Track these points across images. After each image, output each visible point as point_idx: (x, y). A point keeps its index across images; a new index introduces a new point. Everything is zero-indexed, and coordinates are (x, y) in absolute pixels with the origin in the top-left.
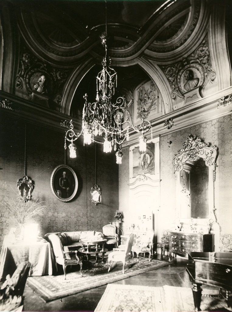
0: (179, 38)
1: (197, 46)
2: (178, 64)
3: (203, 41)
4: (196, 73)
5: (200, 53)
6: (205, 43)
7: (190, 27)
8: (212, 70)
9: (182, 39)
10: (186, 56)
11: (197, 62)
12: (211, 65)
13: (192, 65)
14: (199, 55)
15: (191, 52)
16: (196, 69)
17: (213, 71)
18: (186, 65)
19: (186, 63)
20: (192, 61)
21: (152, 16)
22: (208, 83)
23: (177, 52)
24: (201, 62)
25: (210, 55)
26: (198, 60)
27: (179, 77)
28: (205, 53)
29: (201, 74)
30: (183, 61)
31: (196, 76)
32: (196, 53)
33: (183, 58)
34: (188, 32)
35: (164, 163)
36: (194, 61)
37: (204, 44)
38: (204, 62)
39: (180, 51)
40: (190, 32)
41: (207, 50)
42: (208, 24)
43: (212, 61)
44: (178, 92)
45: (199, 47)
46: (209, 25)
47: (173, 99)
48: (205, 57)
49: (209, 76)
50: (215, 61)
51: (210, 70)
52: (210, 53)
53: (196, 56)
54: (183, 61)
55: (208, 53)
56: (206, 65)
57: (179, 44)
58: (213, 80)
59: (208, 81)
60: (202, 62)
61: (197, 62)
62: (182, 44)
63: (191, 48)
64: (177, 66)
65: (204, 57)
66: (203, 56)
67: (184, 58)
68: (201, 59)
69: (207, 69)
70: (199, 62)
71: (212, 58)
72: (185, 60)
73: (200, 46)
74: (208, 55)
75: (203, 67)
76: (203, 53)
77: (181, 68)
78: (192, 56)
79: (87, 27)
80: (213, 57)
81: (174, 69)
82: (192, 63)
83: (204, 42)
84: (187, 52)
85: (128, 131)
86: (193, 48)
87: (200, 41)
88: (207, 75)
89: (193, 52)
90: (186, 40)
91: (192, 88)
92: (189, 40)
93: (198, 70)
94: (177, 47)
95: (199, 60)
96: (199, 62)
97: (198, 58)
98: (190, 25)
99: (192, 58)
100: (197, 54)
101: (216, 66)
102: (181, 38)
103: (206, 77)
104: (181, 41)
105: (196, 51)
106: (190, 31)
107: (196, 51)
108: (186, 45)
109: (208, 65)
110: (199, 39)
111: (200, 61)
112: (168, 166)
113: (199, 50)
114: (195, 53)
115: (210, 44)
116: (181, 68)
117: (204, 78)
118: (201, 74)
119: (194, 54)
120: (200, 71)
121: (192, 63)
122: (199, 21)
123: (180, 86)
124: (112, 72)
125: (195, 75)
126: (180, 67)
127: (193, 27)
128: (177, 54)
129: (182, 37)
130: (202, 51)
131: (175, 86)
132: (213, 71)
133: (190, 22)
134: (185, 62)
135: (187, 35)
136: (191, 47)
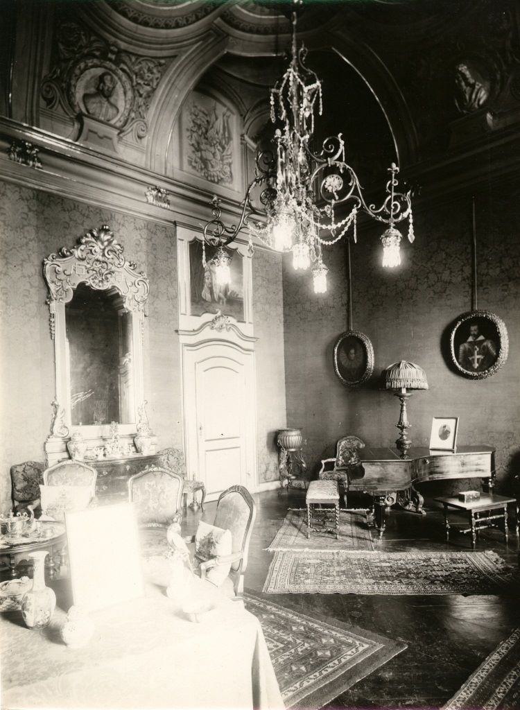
0: (142, 6)
1: (149, 55)
2: (98, 41)
3: (163, 58)
4: (117, 95)
5: (146, 71)
6: (162, 65)
7: (170, 17)
8: (144, 118)
9: (143, 13)
10: (123, 45)
11: (131, 79)
12: (148, 109)
13: (120, 72)
14: (142, 72)
15: (136, 52)
16: (122, 89)
17: (145, 120)
18: (110, 60)
19: (113, 57)
20: (125, 68)
21: (364, 79)
22: (130, 134)
23: (118, 20)
24: (136, 86)
25: (156, 91)
26: (134, 77)
27: (82, 65)
28: (152, 80)
29: (126, 105)
30: (112, 48)
31: (116, 100)
32: (140, 63)
33: (115, 42)
34: (161, 19)
35: (290, 308)
36: (128, 71)
37: (160, 65)
38: (141, 92)
39: (122, 26)
40: (162, 24)
41: (157, 79)
42: (190, 47)
43: (152, 103)
44: (63, 92)
45: (152, 61)
46: (186, 52)
47: (45, 99)
48: (148, 85)
49: (135, 124)
50: (157, 108)
51: (142, 113)
52: (159, 87)
53: (136, 68)
54: (112, 48)
55: (155, 84)
56: (140, 99)
57: (131, 15)
58: (140, 137)
59: (132, 130)
60: (138, 87)
61: (131, 79)
62: (135, 20)
63: (141, 47)
64: (94, 41)
65: (146, 83)
66: (146, 80)
67: (115, 45)
68: (140, 81)
69: (139, 107)
70: (135, 83)
71: (154, 103)
72: (116, 50)
73: (153, 60)
74: (152, 87)
75: (135, 97)
76: (148, 76)
77: (97, 53)
78: (131, 60)
79: (489, 116)
80: (157, 99)
81: (84, 41)
82: (123, 70)
83: (163, 61)
84: (130, 43)
85: (316, 224)
86: (142, 50)
87: (159, 54)
88: (133, 119)
89: (138, 56)
90: (146, 24)
91: (103, 119)
92: (150, 31)
93: (125, 93)
94: (125, 14)
95: (136, 78)
96: (135, 83)
97: (136, 74)
98: (173, 14)
99: (128, 62)
100: (140, 65)
101: (154, 115)
102: (144, 10)
103: (129, 121)
104: (139, 15)
105: (142, 59)
106: (163, 22)
107: (143, 60)
108: (139, 32)
109: (144, 104)
110: (161, 49)
111: (136, 81)
112: (297, 314)
113: (147, 64)
114: (138, 61)
115: (167, 76)
116: (97, 53)
117: (128, 119)
118: (126, 105)
119: (137, 59)
120: (127, 99)
121: (123, 70)
122: (186, 28)
123: (75, 86)
124: (310, 81)
125: (116, 97)
126: (98, 49)
127: (173, 24)
128: (113, 22)
129: (147, 12)
130: (150, 70)
131: (61, 73)
132: (145, 120)
133: (177, 13)
134: (113, 52)
135: (155, 20)
136: (141, 43)
